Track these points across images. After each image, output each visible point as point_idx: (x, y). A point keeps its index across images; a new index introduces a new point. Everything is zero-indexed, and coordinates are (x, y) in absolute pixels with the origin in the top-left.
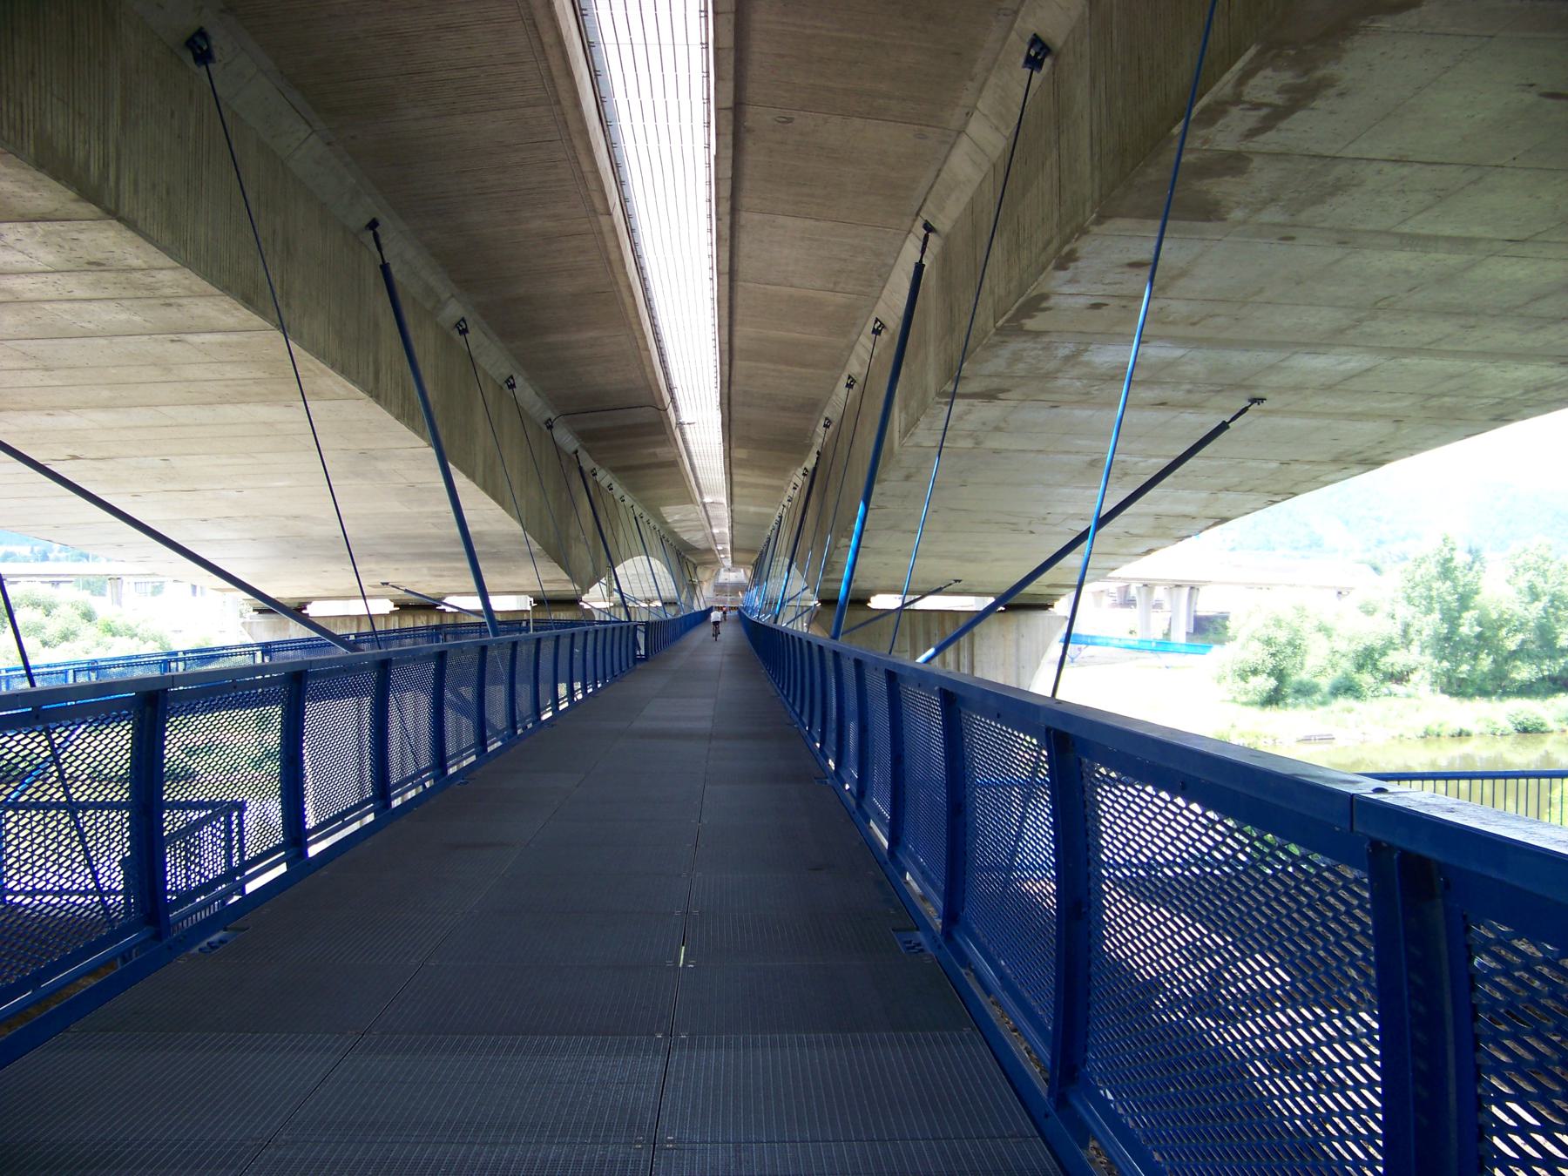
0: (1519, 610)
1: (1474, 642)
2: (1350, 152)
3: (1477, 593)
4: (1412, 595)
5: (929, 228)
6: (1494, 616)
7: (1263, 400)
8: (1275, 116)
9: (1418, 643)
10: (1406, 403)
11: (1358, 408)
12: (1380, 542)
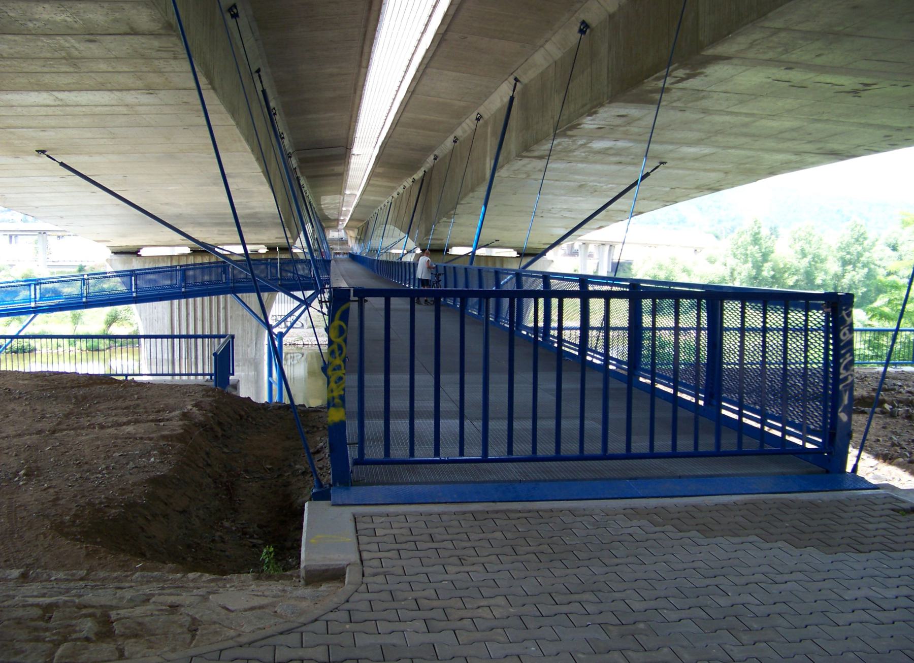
0: (796, 263)
1: (771, 280)
2: (709, 89)
3: (772, 253)
4: (736, 253)
5: (516, 80)
6: (781, 266)
7: (666, 163)
8: (682, 80)
9: (739, 280)
10: (729, 166)
11: (708, 167)
12: (720, 221)
